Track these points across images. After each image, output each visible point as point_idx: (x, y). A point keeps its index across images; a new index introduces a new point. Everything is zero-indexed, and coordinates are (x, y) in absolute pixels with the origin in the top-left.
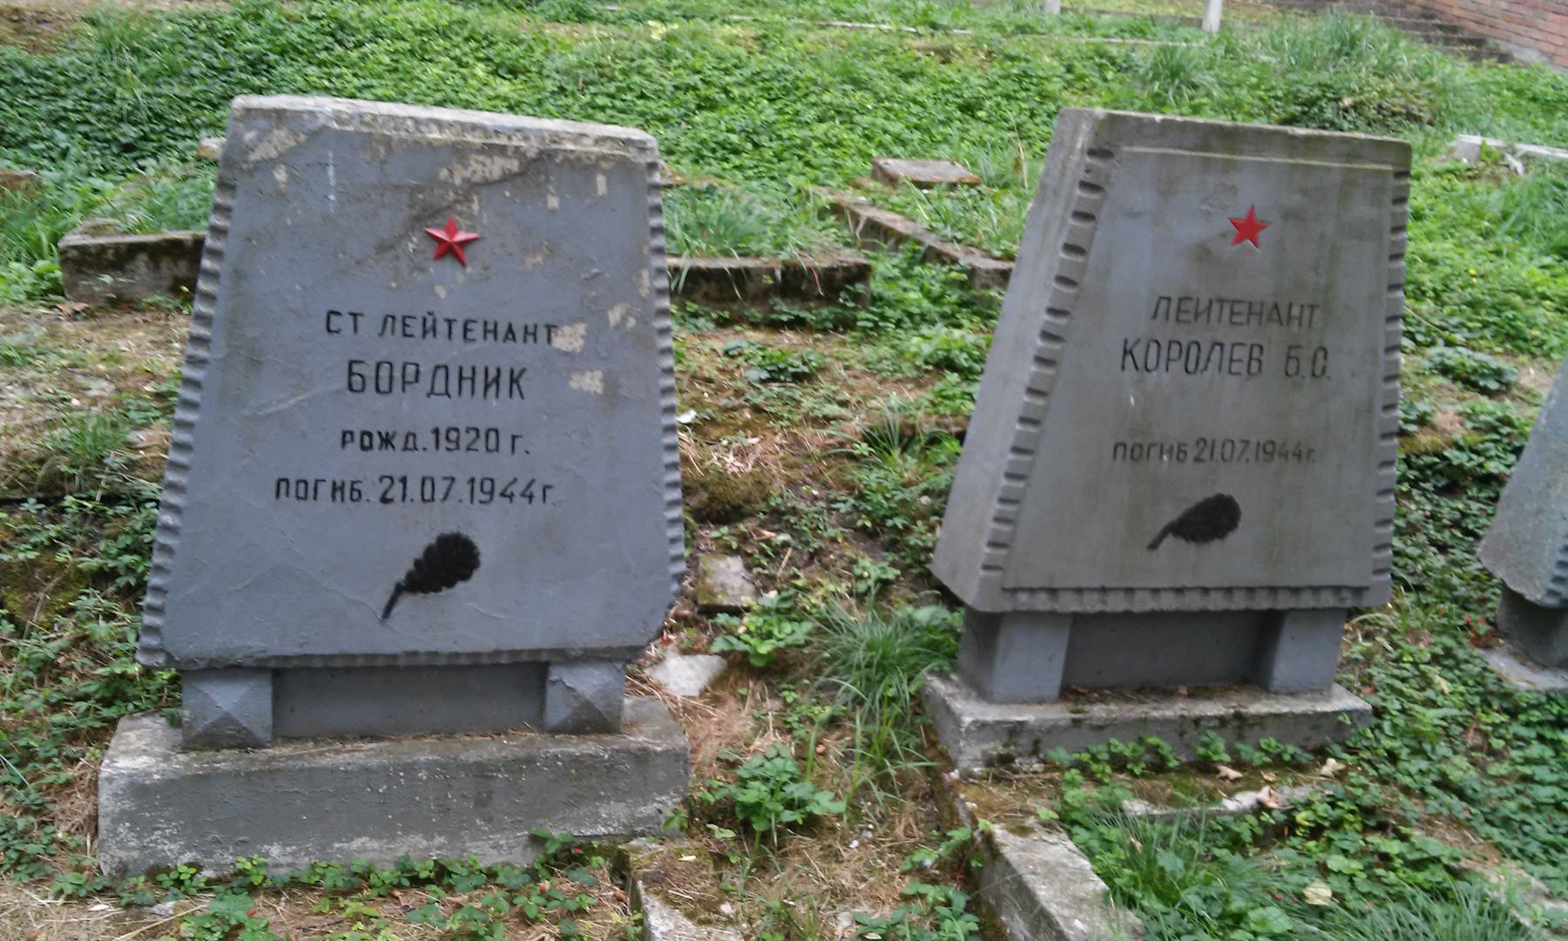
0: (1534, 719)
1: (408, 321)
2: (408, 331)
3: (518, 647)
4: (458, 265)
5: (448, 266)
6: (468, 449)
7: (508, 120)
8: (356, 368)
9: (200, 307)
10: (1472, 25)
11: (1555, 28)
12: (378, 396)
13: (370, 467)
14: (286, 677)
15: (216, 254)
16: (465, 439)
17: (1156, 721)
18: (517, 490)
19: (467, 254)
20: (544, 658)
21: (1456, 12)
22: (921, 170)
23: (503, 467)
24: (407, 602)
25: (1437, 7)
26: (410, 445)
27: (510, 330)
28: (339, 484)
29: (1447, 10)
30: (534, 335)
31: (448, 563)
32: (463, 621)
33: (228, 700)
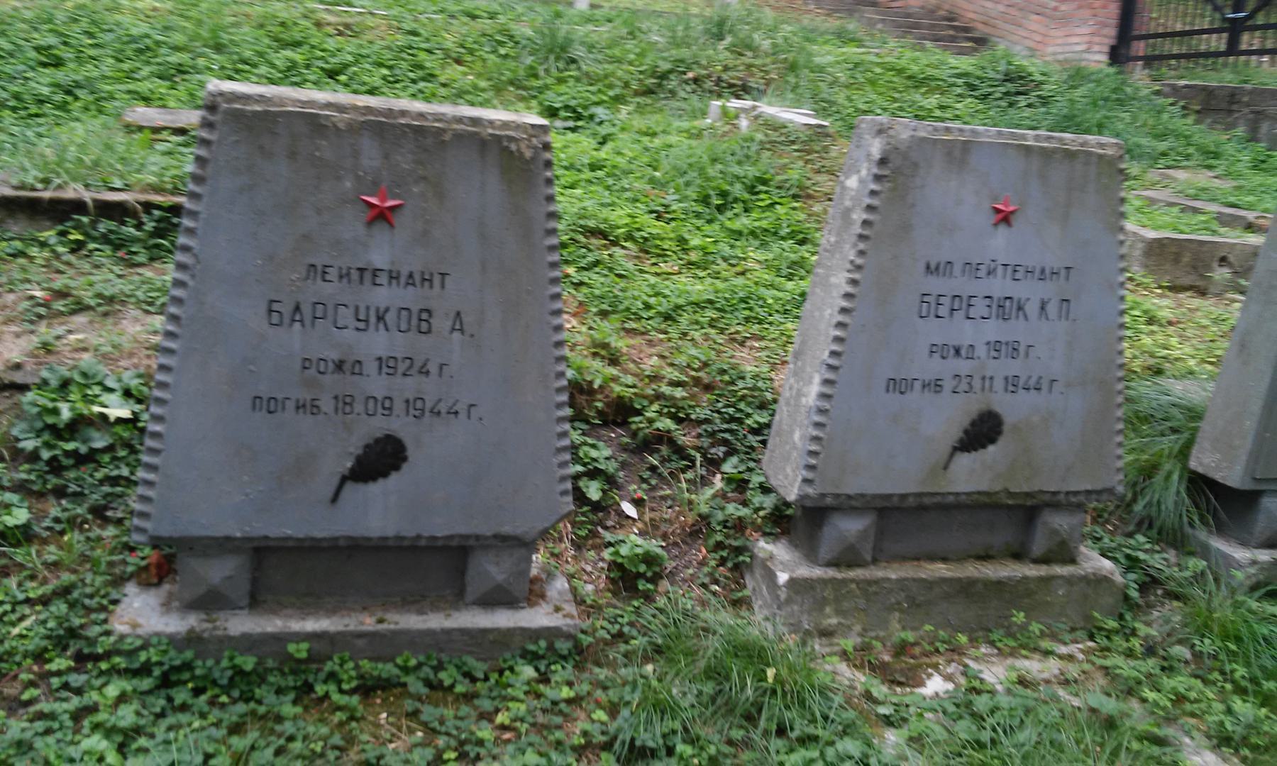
0: (63, 667)
1: (327, 270)
2: (328, 277)
3: (337, 534)
4: (386, 226)
5: (380, 229)
6: (405, 375)
7: (372, 101)
8: (275, 307)
9: (180, 257)
10: (980, 26)
11: (1034, 27)
12: (434, 329)
13: (945, 368)
14: (262, 553)
15: (193, 214)
16: (402, 367)
17: (1062, 577)
18: (443, 407)
19: (397, 219)
20: (472, 542)
21: (971, 15)
22: (169, 117)
23: (430, 389)
24: (349, 487)
25: (958, 11)
26: (357, 370)
27: (411, 276)
28: (301, 403)
29: (963, 13)
30: (430, 281)
31: (381, 459)
32: (378, 511)
33: (218, 571)
